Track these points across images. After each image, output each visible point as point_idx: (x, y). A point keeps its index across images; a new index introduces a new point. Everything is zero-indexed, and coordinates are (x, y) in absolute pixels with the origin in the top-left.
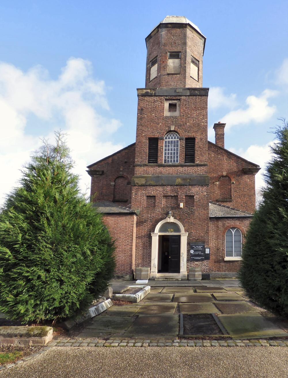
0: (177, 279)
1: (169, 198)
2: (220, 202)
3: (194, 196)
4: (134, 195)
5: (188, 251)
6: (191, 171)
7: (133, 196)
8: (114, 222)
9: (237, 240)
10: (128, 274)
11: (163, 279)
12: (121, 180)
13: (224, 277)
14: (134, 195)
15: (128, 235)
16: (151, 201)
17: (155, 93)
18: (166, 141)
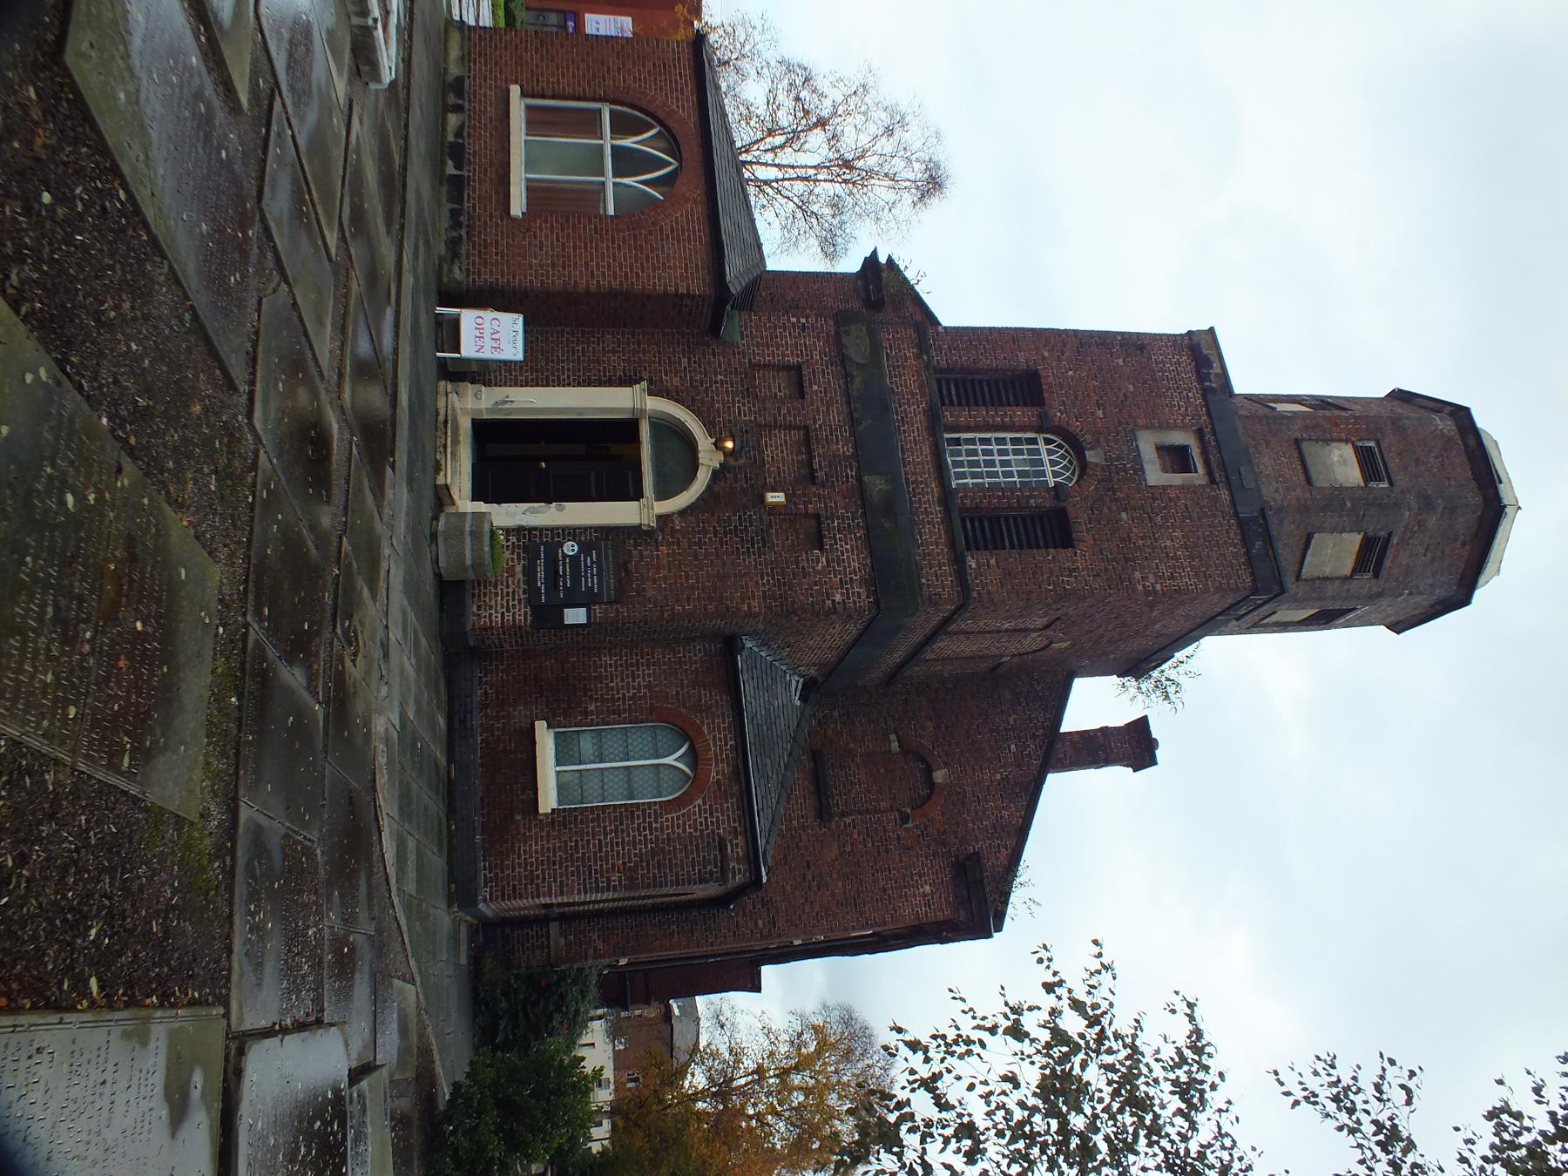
0: (443, 467)
1: (799, 453)
2: (812, 765)
4: (798, 321)
5: (572, 532)
6: (931, 537)
7: (794, 320)
9: (636, 786)
10: (468, 276)
11: (442, 412)
13: (457, 725)
14: (798, 321)
16: (780, 386)
18: (1037, 444)
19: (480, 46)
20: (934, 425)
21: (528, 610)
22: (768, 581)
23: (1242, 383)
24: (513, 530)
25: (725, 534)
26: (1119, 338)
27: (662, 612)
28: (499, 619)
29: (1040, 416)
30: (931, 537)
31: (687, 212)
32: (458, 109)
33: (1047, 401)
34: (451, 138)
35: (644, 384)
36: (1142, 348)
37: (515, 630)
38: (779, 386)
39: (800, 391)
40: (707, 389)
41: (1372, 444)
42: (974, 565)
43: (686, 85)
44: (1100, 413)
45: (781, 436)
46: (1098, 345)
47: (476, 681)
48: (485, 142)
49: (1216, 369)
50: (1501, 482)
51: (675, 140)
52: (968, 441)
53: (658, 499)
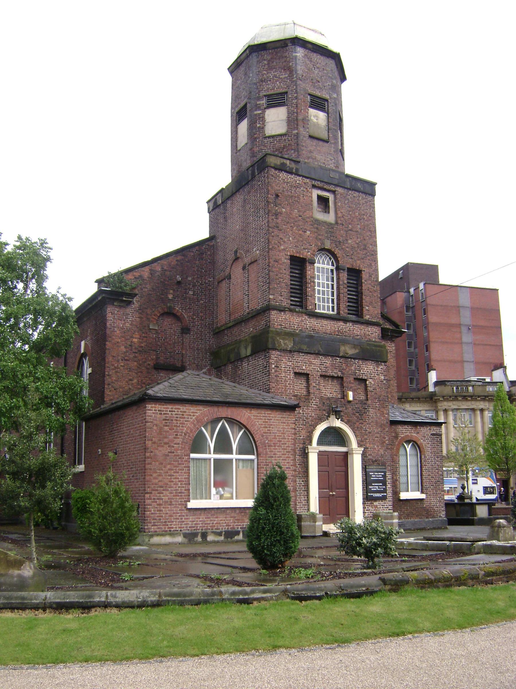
7: (273, 370)
8: (264, 422)
12: (169, 320)
14: (274, 368)
15: (289, 449)
17: (297, 170)
19: (159, 525)
31: (256, 419)
32: (204, 535)
34: (222, 538)
43: (179, 409)
48: (221, 520)
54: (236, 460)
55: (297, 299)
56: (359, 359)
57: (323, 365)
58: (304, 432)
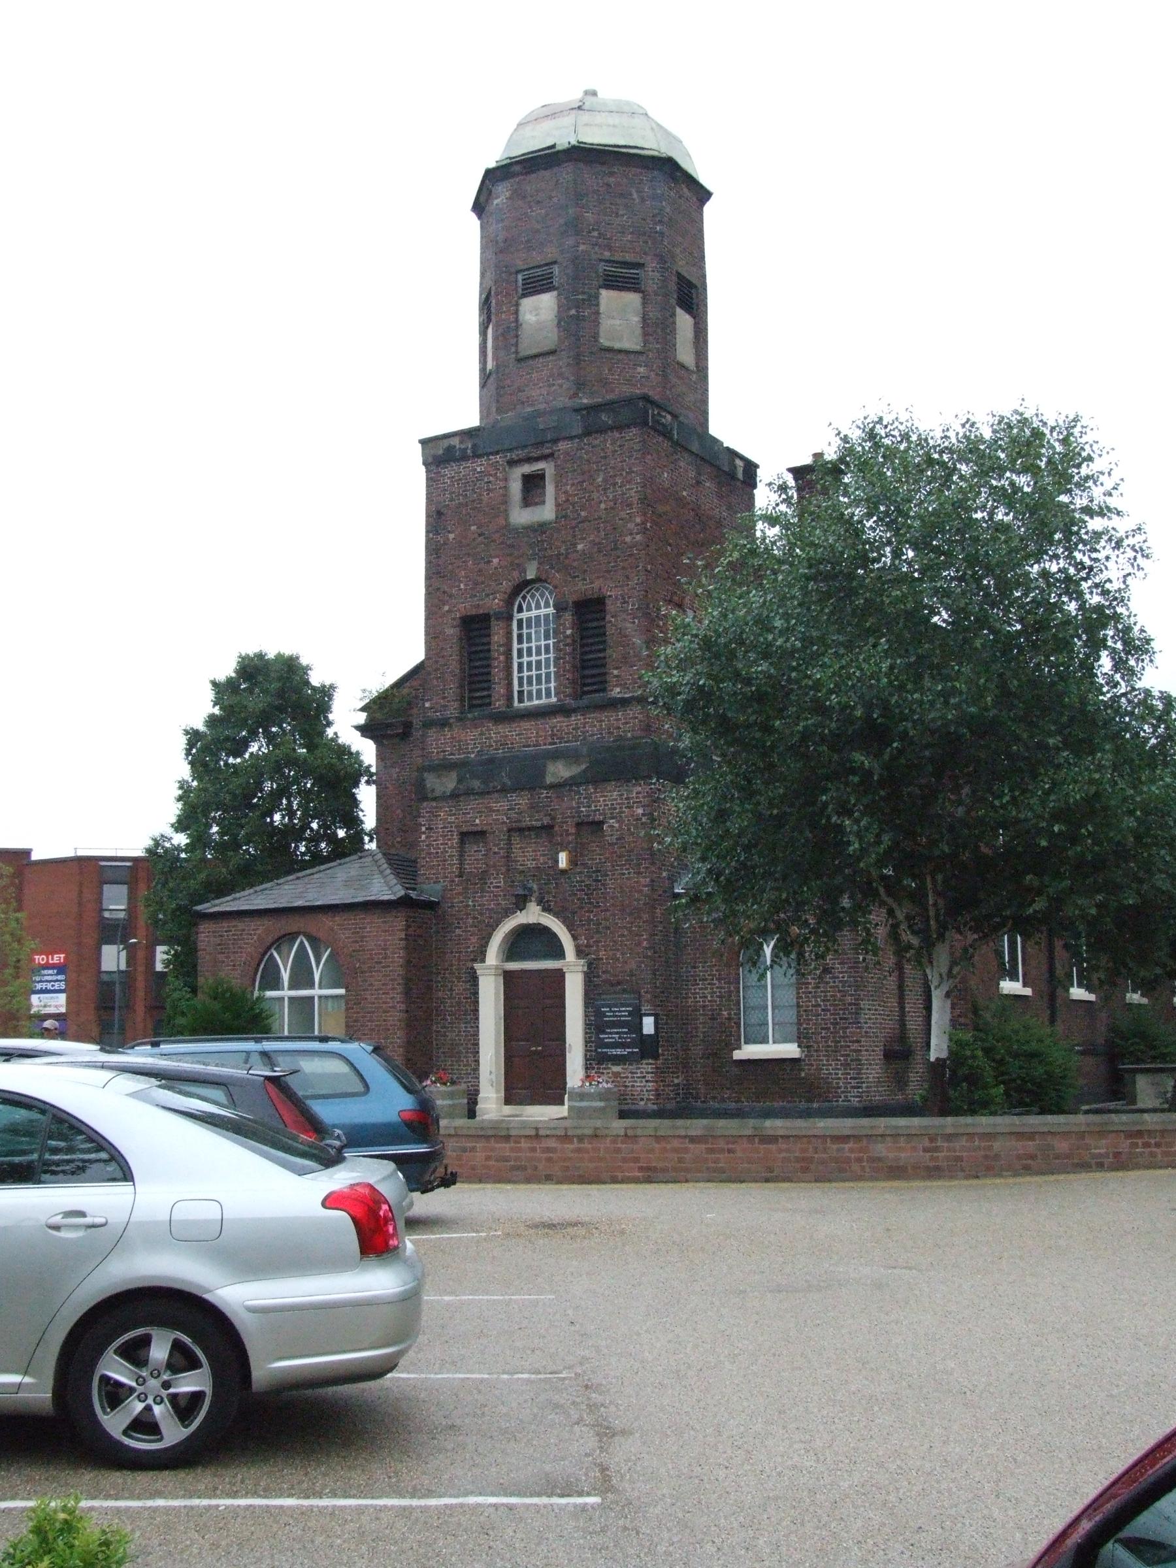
3: (601, 823)
4: (424, 833)
7: (423, 837)
20: (510, 717)
21: (644, 1062)
22: (627, 869)
23: (470, 417)
24: (586, 1072)
25: (591, 903)
26: (431, 535)
27: (646, 957)
28: (651, 1084)
29: (498, 619)
30: (595, 726)
33: (486, 612)
35: (476, 966)
36: (439, 513)
37: (660, 1073)
38: (476, 854)
39: (480, 835)
40: (479, 914)
41: (520, 277)
42: (618, 690)
44: (495, 561)
45: (516, 852)
46: (438, 557)
47: (705, 1105)
49: (455, 442)
50: (553, 146)
51: (285, 936)
52: (521, 684)
53: (564, 958)
54: (289, 998)
55: (591, 656)
56: (587, 782)
57: (514, 809)
58: (474, 939)
